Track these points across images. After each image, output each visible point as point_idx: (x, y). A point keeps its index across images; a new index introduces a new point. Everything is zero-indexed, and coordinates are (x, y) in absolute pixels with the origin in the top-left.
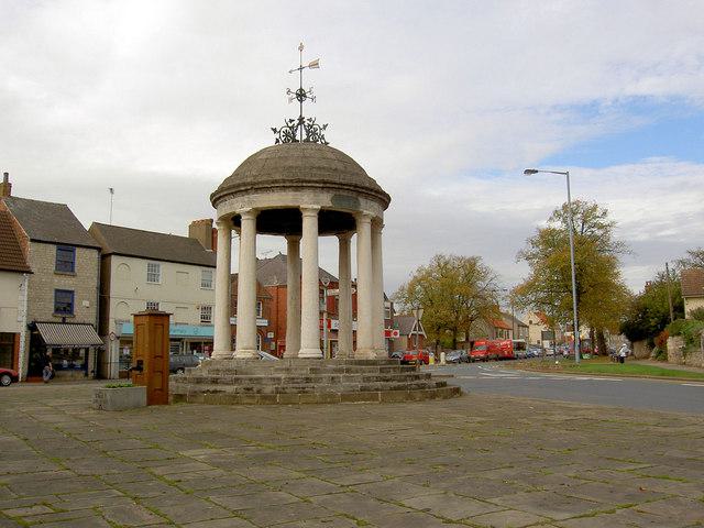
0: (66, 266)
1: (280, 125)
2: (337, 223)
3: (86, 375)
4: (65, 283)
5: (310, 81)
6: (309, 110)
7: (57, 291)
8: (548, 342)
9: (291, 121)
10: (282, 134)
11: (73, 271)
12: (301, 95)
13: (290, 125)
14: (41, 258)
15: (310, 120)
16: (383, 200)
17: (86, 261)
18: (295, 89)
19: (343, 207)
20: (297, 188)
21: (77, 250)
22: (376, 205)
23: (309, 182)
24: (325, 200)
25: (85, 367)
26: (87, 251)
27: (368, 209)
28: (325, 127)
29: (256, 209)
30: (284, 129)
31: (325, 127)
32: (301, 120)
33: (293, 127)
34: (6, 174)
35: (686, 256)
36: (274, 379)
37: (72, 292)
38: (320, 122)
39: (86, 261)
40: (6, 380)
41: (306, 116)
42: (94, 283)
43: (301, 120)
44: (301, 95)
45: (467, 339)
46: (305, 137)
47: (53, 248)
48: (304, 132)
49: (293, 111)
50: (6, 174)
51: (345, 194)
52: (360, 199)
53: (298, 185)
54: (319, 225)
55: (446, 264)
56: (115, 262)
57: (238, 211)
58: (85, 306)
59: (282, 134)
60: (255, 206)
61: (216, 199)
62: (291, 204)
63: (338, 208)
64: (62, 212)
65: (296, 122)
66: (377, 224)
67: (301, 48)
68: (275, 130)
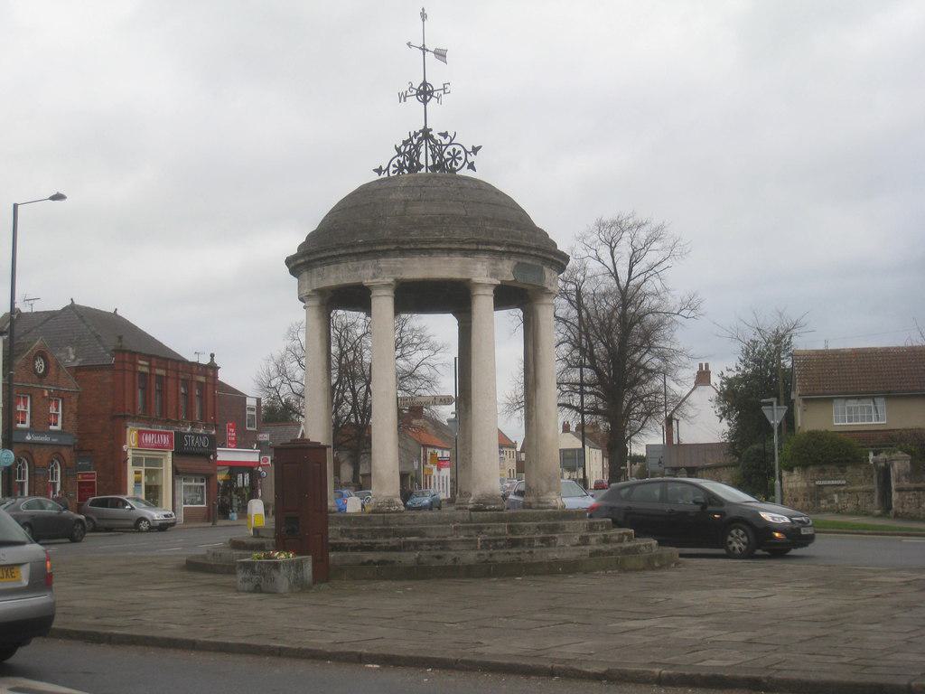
6: (439, 117)
28: (475, 150)
29: (396, 280)
31: (475, 150)
44: (425, 93)
49: (410, 117)
57: (367, 282)
60: (399, 276)
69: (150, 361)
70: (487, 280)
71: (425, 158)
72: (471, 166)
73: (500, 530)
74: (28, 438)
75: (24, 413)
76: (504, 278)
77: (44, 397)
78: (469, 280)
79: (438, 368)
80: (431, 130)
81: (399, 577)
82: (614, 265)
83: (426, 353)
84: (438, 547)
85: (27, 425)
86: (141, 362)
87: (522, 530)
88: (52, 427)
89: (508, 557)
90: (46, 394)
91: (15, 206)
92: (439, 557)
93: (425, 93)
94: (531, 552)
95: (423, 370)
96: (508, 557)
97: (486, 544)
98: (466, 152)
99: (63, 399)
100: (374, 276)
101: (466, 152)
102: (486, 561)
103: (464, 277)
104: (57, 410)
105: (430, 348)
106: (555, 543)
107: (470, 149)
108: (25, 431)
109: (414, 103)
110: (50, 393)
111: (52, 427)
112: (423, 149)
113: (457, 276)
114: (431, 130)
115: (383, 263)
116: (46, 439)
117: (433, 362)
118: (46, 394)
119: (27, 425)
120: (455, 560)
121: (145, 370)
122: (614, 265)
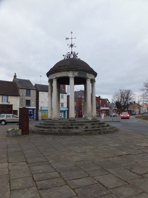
0: (28, 94)
1: (65, 54)
2: (79, 81)
3: (34, 120)
4: (28, 98)
5: (74, 42)
6: (74, 50)
9: (69, 53)
10: (66, 56)
11: (30, 95)
12: (72, 46)
13: (69, 54)
14: (23, 92)
15: (74, 52)
16: (95, 74)
17: (33, 93)
18: (70, 44)
19: (82, 76)
20: (67, 71)
21: (31, 90)
22: (92, 75)
23: (71, 69)
24: (76, 74)
25: (33, 118)
26: (33, 91)
27: (90, 76)
28: (78, 54)
29: (56, 78)
30: (67, 55)
33: (69, 55)
34: (15, 73)
36: (59, 127)
38: (76, 53)
39: (33, 93)
40: (3, 123)
41: (73, 51)
42: (35, 98)
43: (72, 53)
45: (128, 110)
47: (26, 90)
50: (15, 73)
51: (82, 72)
52: (87, 73)
53: (68, 70)
54: (69, 82)
55: (122, 92)
56: (40, 93)
57: (52, 78)
58: (33, 103)
59: (66, 56)
61: (48, 74)
62: (66, 75)
63: (80, 76)
64: (28, 82)
65: (70, 53)
66: (93, 81)
67: (72, 33)
68: (64, 55)
72: (77, 57)
73: (69, 125)
87: (73, 125)
97: (63, 128)
112: (71, 56)
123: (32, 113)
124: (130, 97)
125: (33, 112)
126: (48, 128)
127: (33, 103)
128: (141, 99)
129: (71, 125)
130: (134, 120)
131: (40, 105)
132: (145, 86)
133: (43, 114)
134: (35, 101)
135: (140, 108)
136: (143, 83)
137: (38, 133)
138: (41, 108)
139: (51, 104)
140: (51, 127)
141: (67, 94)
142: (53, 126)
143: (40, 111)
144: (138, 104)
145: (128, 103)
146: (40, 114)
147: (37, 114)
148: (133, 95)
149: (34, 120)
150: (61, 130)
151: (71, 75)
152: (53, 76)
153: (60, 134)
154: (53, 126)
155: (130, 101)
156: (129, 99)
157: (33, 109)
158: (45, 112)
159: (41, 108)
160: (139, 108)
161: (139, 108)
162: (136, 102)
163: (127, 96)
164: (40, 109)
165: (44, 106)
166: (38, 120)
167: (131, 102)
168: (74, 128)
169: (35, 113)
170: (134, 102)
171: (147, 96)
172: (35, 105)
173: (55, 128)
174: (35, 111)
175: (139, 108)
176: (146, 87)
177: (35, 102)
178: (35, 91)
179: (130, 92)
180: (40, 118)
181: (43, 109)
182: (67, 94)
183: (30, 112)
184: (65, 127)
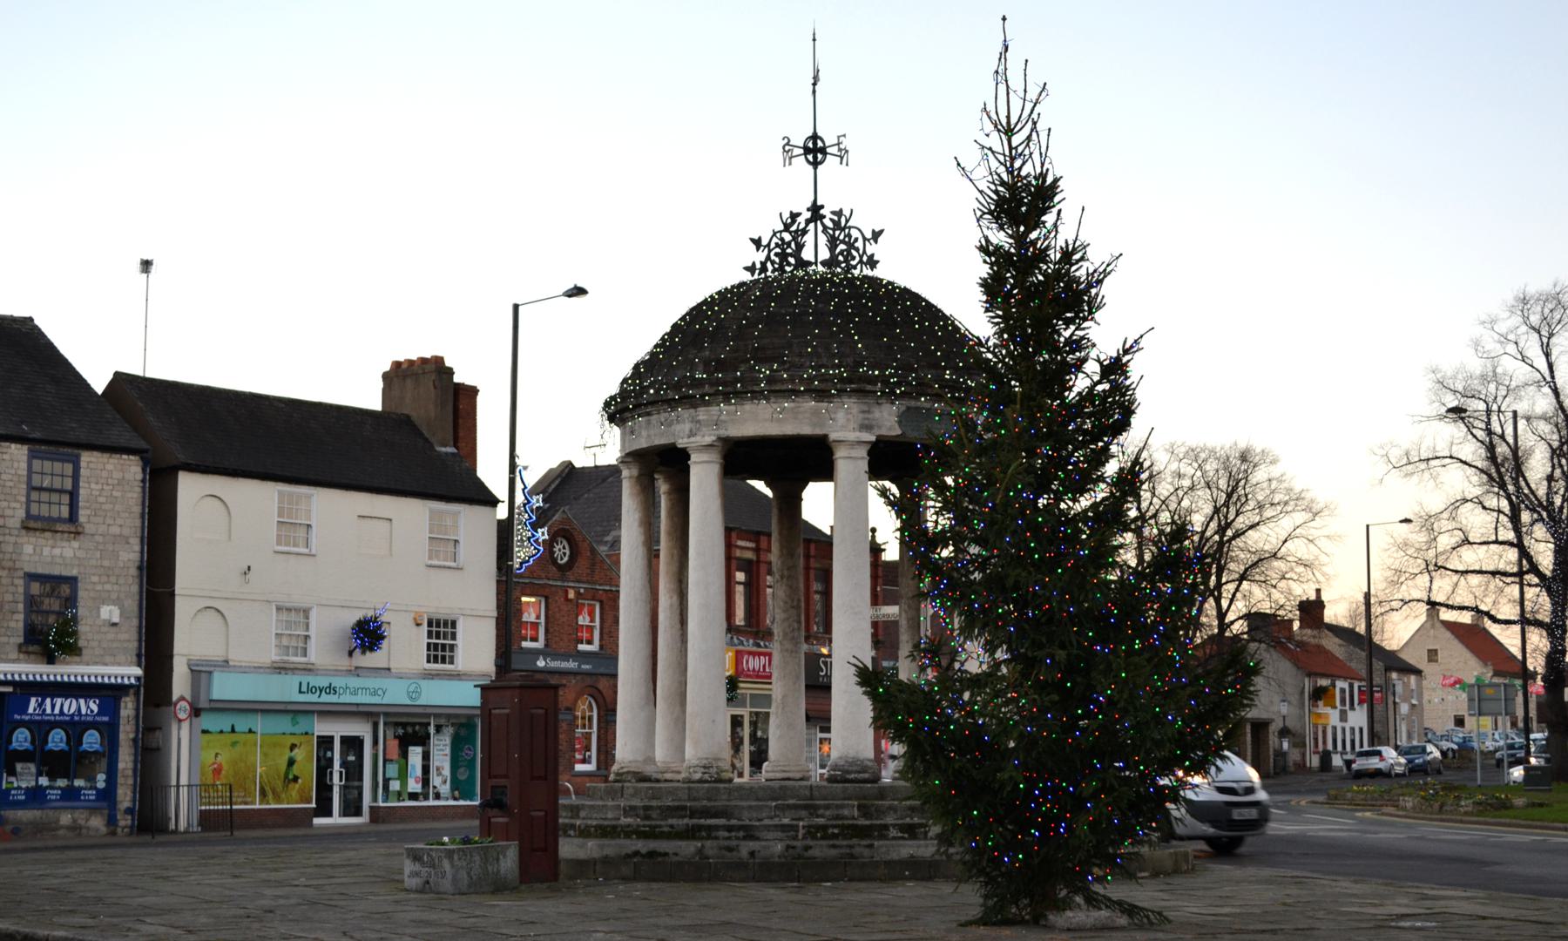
1: (768, 226)
4: (51, 554)
6: (838, 188)
7: (31, 577)
8: (973, 667)
9: (794, 216)
15: (839, 213)
18: (799, 140)
20: (821, 395)
24: (888, 420)
28: (876, 235)
29: (720, 439)
31: (876, 235)
32: (816, 210)
35: (1104, 335)
36: (783, 828)
37: (72, 581)
38: (863, 222)
39: (111, 482)
42: (131, 554)
43: (816, 210)
44: (815, 151)
46: (824, 254)
48: (822, 239)
49: (793, 189)
56: (191, 489)
57: (682, 443)
58: (108, 614)
60: (723, 433)
61: (619, 410)
69: (757, 542)
70: (853, 436)
71: (815, 249)
72: (872, 263)
73: (846, 812)
74: (541, 663)
75: (535, 626)
76: (884, 432)
77: (567, 599)
78: (826, 436)
79: (1322, 543)
80: (822, 207)
81: (670, 878)
82: (1551, 366)
83: (1299, 517)
84: (741, 834)
85: (540, 645)
86: (740, 543)
87: (881, 812)
88: (582, 647)
89: (834, 852)
90: (571, 595)
91: (516, 307)
92: (730, 849)
93: (815, 151)
94: (871, 846)
95: (1296, 548)
96: (834, 852)
97: (812, 832)
98: (865, 239)
99: (601, 603)
100: (692, 434)
101: (865, 239)
102: (800, 857)
103: (818, 431)
104: (592, 620)
105: (1308, 509)
106: (926, 833)
107: (869, 235)
108: (536, 653)
109: (801, 165)
110: (578, 594)
111: (582, 647)
112: (809, 239)
113: (806, 430)
114: (822, 207)
115: (702, 414)
116: (571, 665)
117: (1313, 533)
118: (571, 595)
119: (540, 645)
120: (752, 854)
121: (750, 555)
122: (1551, 366)
123: (91, 740)
124: (1258, 540)
125: (110, 732)
126: (690, 834)
127: (110, 612)
128: (1398, 577)
129: (865, 811)
130: (1314, 822)
131: (191, 639)
132: (1458, 412)
133: (220, 754)
134: (129, 588)
135: (1388, 688)
136: (1428, 383)
137: (626, 870)
138: (200, 673)
139: (647, 652)
140: (717, 828)
141: (493, 502)
142: (722, 821)
143: (183, 711)
144: (1362, 641)
145: (1223, 626)
146: (186, 754)
147: (151, 756)
148: (1286, 524)
149: (112, 821)
150: (807, 848)
151: (848, 425)
152: (698, 431)
153: (794, 870)
154: (722, 821)
155: (1258, 598)
156: (1235, 568)
157: (109, 694)
158: (242, 723)
159: (200, 673)
160: (1374, 698)
161: (1374, 698)
162: (1335, 613)
163: (1221, 530)
164: (180, 685)
165: (237, 656)
166: (164, 830)
167: (1266, 608)
168: (893, 833)
169: (126, 732)
170: (1312, 610)
171: (1467, 541)
172: (129, 637)
173: (750, 834)
174: (127, 708)
175: (1368, 698)
176: (1457, 430)
177: (132, 604)
178: (132, 469)
179: (1259, 475)
180: (183, 809)
181: (224, 688)
182: (502, 512)
183: (76, 728)
184: (824, 828)
